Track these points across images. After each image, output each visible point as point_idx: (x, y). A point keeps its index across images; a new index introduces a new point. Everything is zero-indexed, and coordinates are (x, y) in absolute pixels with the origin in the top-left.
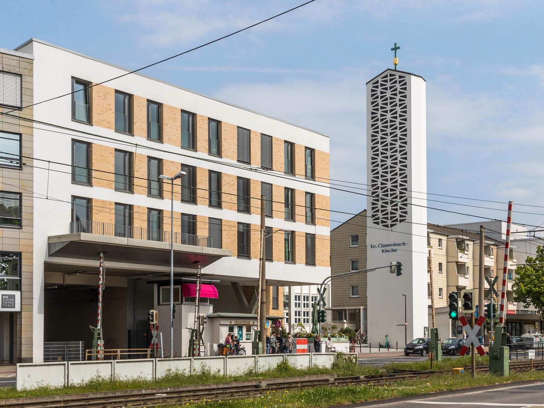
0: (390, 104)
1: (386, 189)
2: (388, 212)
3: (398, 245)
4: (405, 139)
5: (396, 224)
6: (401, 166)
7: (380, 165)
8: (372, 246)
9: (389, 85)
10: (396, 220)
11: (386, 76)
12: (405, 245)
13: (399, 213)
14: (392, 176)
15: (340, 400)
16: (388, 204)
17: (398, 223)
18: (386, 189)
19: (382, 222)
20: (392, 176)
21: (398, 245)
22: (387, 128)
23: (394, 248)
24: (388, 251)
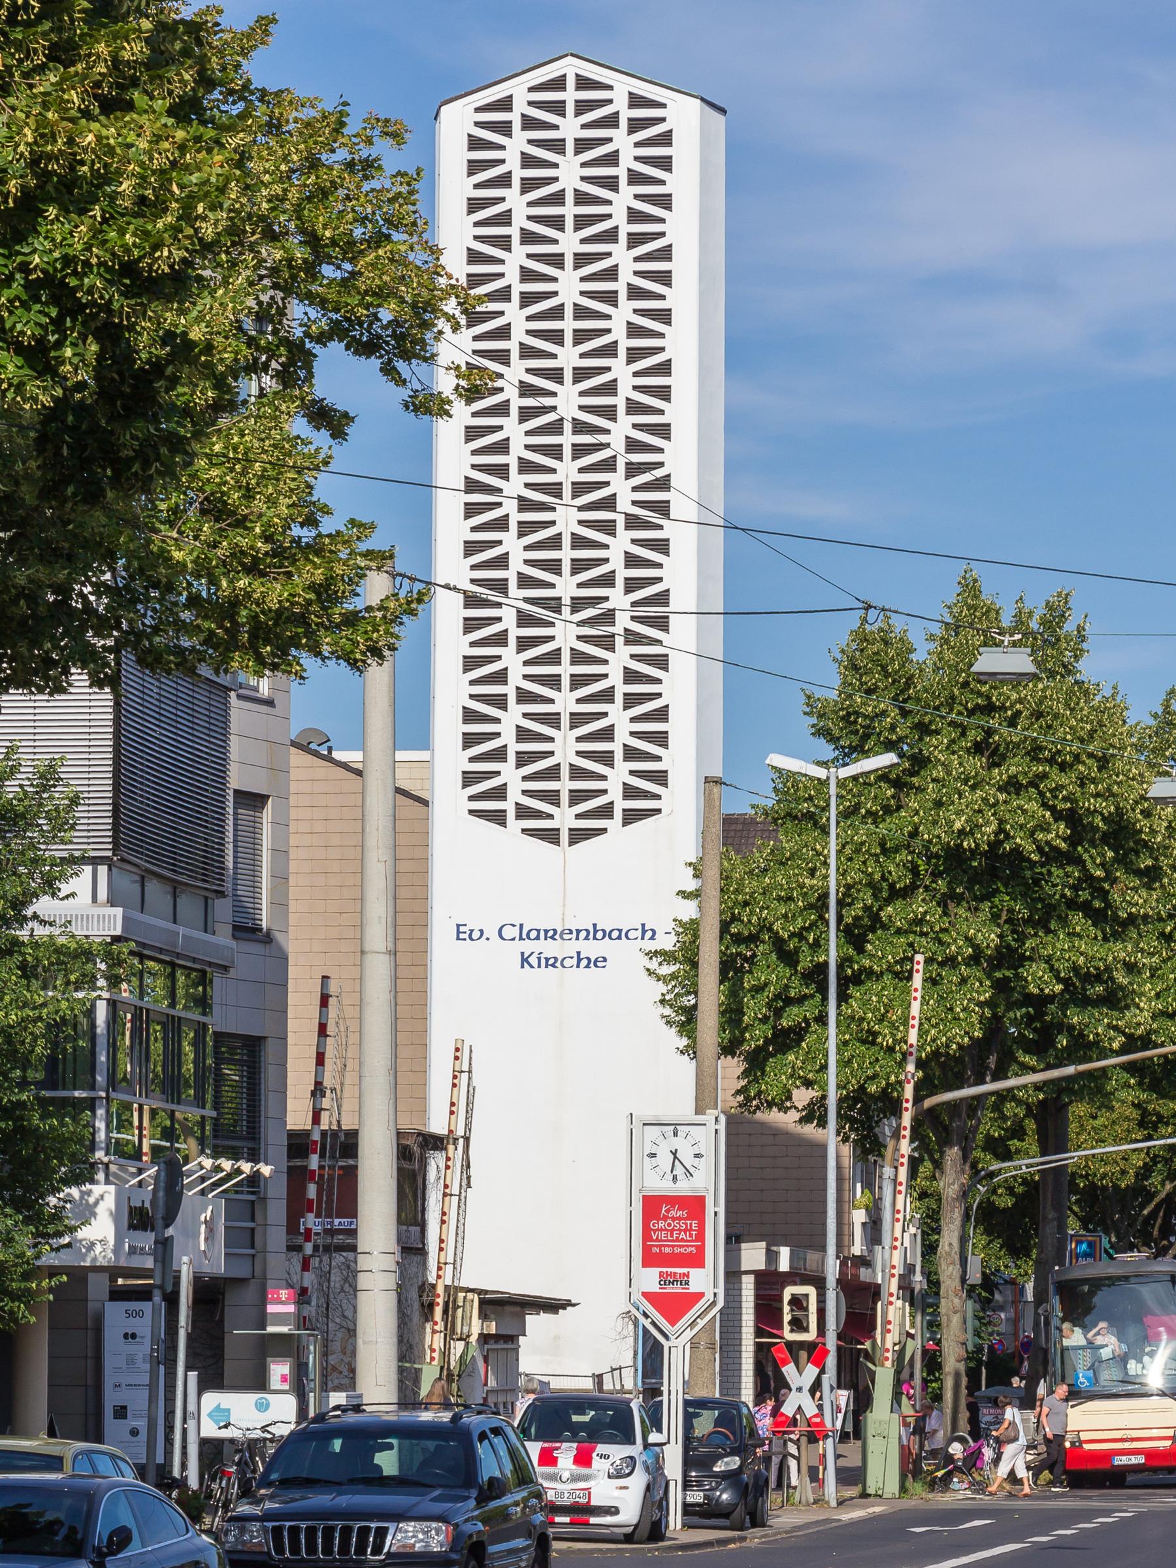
0: (573, 802)
1: (550, 417)
2: (578, 113)
3: (615, 934)
8: (461, 932)
13: (619, 774)
16: (563, 115)
18: (550, 417)
21: (615, 934)
22: (560, 382)
23: (591, 949)
24: (551, 963)
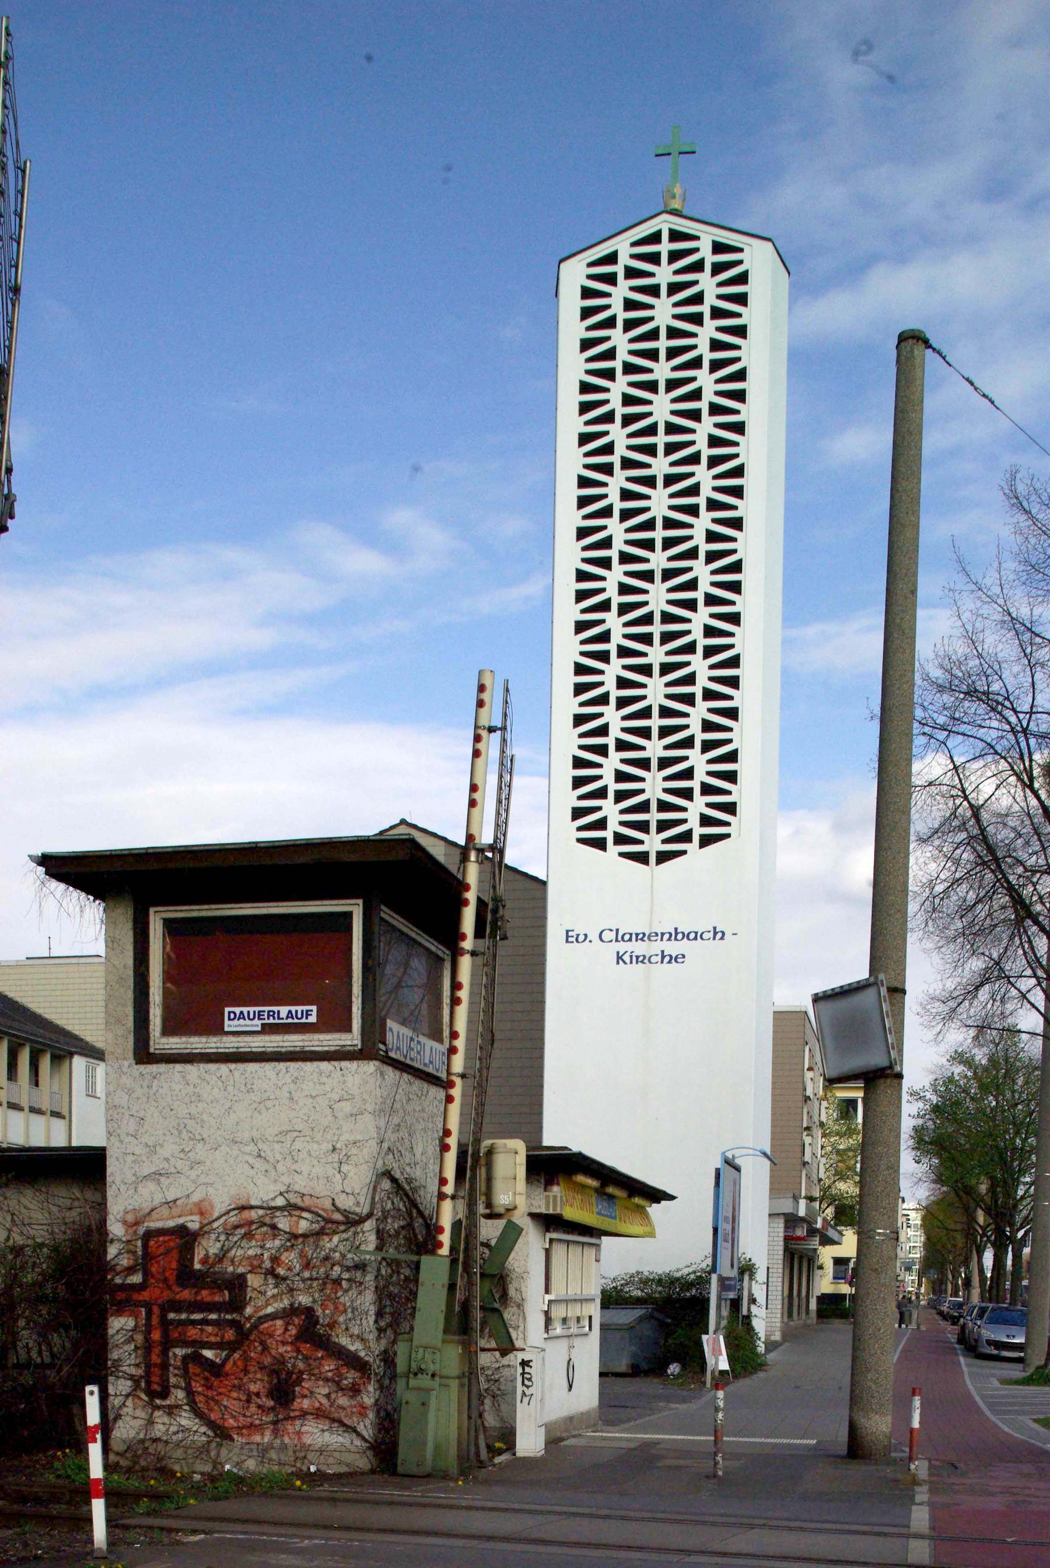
2: (653, 520)
3: (692, 936)
4: (735, 508)
5: (684, 852)
6: (719, 329)
7: (620, 324)
9: (664, 274)
10: (686, 837)
11: (655, 238)
12: (722, 938)
13: (698, 806)
14: (666, 748)
15: (387, 1321)
17: (693, 847)
19: (620, 839)
20: (675, 369)
21: (692, 936)
22: (650, 675)
23: (672, 948)
24: (641, 959)
